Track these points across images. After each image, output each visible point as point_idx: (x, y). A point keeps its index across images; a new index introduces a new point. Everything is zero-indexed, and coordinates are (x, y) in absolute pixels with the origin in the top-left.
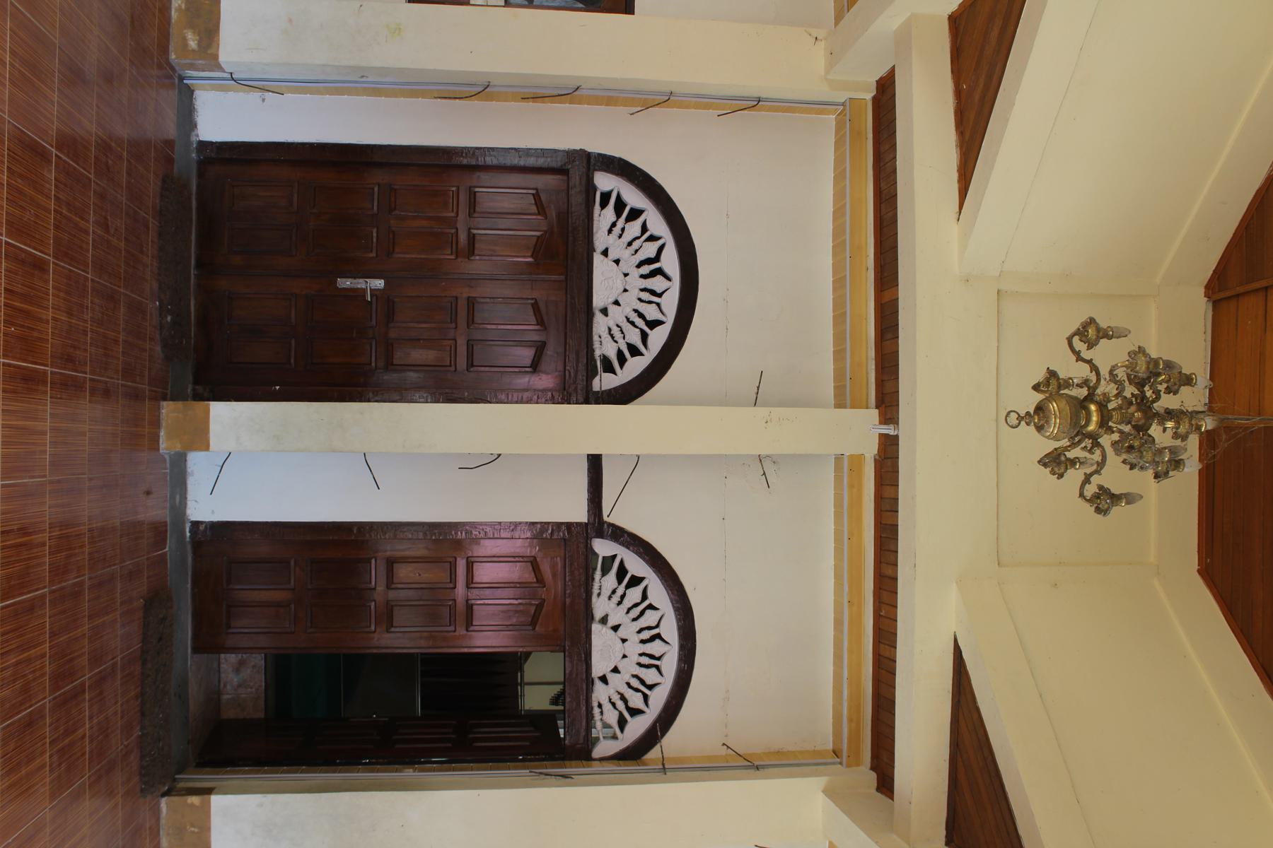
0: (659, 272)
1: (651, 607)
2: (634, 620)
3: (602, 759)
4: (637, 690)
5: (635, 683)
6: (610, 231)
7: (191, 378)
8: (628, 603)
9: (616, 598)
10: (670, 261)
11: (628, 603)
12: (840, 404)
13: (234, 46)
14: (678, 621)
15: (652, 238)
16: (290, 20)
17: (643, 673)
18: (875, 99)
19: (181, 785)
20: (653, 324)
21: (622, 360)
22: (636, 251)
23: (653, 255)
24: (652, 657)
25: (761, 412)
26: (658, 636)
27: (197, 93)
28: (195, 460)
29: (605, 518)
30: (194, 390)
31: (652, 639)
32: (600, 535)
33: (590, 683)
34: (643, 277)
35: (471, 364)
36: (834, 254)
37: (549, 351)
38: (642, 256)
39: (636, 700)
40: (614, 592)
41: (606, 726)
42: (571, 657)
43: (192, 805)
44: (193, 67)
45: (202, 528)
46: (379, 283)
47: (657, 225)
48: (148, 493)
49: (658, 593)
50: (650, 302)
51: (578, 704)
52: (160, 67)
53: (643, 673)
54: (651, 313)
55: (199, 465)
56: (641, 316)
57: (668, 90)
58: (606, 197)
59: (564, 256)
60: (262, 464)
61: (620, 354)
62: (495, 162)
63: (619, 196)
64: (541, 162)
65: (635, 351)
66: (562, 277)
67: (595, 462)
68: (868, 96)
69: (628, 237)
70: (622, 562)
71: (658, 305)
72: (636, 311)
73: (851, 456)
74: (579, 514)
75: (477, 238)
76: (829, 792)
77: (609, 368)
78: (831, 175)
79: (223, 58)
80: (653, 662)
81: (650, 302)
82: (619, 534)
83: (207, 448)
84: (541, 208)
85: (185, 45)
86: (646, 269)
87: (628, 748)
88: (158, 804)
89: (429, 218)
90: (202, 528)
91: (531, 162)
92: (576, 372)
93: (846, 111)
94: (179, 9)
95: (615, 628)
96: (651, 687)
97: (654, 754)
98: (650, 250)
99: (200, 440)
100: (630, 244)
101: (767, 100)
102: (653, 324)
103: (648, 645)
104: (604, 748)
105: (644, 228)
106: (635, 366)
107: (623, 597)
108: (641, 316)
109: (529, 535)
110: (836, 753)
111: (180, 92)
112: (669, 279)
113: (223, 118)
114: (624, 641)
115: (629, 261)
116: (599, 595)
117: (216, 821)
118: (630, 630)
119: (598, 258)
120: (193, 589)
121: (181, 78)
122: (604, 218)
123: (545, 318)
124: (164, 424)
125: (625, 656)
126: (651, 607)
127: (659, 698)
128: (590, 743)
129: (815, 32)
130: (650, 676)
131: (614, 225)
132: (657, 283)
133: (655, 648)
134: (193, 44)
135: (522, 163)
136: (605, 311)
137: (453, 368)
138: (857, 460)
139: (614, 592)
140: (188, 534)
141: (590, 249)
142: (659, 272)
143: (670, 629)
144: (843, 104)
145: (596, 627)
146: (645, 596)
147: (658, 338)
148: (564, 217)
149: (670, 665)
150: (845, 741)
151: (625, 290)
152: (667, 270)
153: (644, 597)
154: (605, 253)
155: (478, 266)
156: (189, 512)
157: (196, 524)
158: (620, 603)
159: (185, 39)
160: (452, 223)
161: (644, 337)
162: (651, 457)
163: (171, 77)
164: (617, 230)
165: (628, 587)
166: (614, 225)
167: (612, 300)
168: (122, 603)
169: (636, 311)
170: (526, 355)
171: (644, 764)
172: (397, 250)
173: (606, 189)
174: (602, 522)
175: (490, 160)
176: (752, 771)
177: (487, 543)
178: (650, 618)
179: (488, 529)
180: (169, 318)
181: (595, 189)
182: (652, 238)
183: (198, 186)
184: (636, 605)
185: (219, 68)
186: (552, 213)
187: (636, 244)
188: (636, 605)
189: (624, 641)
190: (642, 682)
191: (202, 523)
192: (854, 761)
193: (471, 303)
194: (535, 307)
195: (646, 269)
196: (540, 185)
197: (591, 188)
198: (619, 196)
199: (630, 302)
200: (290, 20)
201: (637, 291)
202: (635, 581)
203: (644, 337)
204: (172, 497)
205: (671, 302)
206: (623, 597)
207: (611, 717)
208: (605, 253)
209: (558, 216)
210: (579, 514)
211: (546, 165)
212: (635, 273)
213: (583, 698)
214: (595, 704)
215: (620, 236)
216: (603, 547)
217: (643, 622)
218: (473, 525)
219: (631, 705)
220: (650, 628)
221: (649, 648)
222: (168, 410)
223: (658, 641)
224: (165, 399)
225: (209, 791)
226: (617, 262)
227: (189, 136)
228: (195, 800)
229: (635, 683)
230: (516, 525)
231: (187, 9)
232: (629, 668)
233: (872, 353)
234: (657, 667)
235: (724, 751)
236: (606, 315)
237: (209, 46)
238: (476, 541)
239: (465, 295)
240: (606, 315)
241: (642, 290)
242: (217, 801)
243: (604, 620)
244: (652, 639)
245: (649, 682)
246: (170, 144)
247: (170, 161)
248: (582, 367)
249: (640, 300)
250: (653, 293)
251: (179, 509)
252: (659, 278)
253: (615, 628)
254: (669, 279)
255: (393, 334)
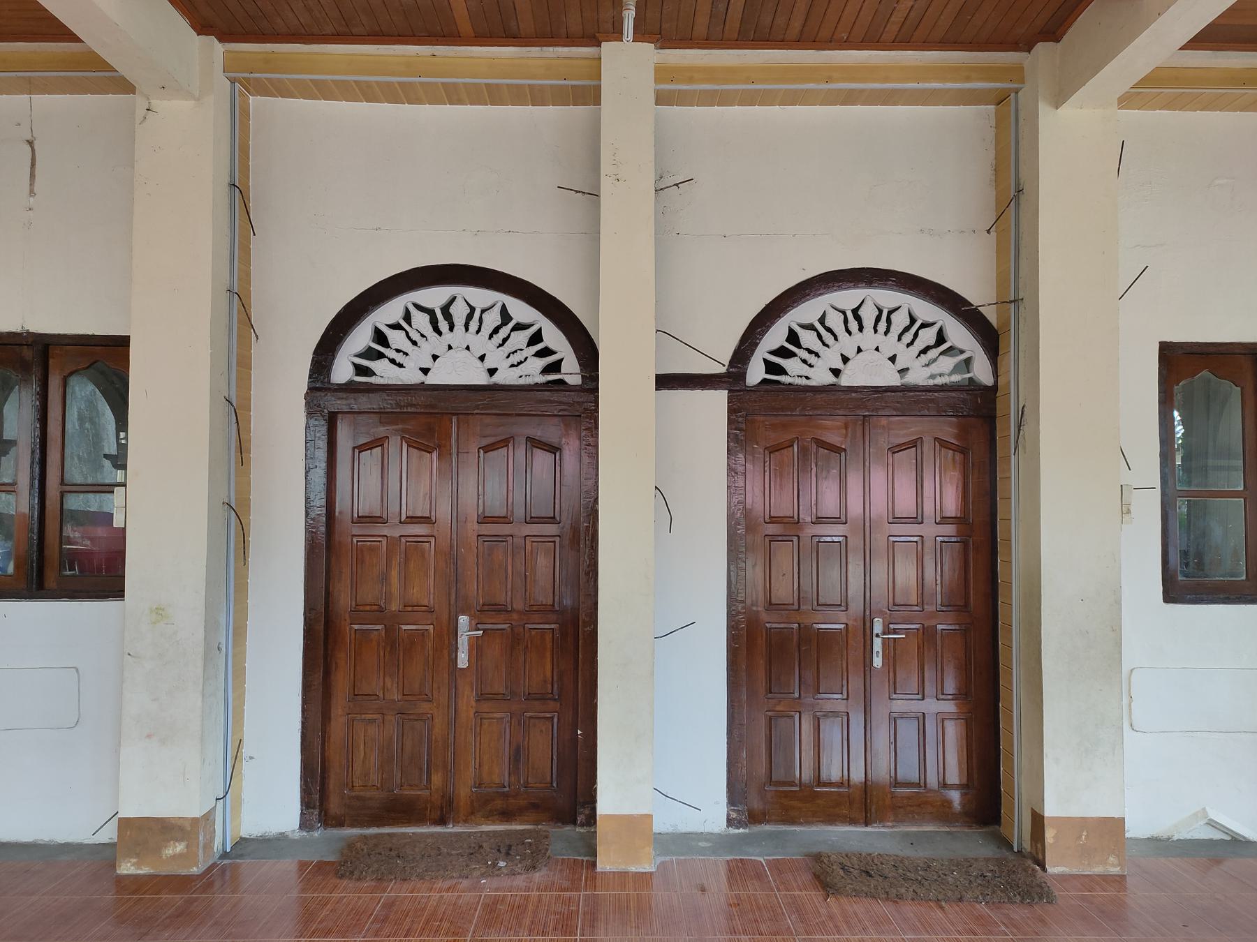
0: (446, 310)
1: (822, 320)
2: (836, 338)
3: (996, 373)
4: (916, 335)
5: (908, 337)
6: (400, 366)
7: (568, 828)
8: (816, 345)
9: (812, 359)
10: (434, 296)
11: (816, 345)
12: (597, 100)
13: (181, 802)
14: (840, 288)
15: (407, 317)
16: (149, 736)
17: (896, 329)
18: (222, 39)
19: (1027, 845)
20: (505, 316)
21: (546, 352)
22: (423, 336)
23: (427, 317)
24: (878, 319)
25: (606, 186)
26: (855, 312)
27: (244, 833)
28: (659, 826)
29: (723, 370)
30: (582, 825)
31: (858, 318)
32: (742, 376)
33: (905, 389)
34: (451, 329)
35: (552, 520)
36: (418, 101)
37: (537, 433)
38: (428, 329)
39: (928, 336)
40: (804, 361)
41: (956, 370)
42: (877, 410)
43: (1055, 837)
44: (208, 845)
45: (734, 815)
46: (463, 620)
47: (390, 311)
48: (703, 890)
49: (807, 312)
50: (481, 320)
51: (932, 401)
52: (210, 885)
53: (896, 329)
54: (493, 319)
55: (668, 820)
56: (496, 331)
57: (225, 296)
58: (361, 370)
59: (432, 417)
60: (663, 755)
61: (539, 354)
62: (323, 495)
63: (359, 356)
64: (322, 443)
65: (536, 338)
66: (454, 419)
67: (665, 382)
68: (218, 48)
69: (406, 346)
70: (772, 353)
71: (483, 311)
72: (491, 337)
73: (657, 80)
74: (718, 399)
75: (410, 514)
76: (1059, 100)
77: (555, 367)
78: (322, 104)
79: (197, 814)
80: (884, 317)
81: (481, 320)
82: (742, 355)
83: (650, 816)
84: (378, 443)
85: (181, 855)
86: (443, 325)
87: (983, 345)
88: (1052, 876)
89: (389, 565)
90: (734, 815)
91: (322, 455)
92: (561, 403)
93: (246, 83)
94: (138, 865)
95: (845, 360)
96: (913, 320)
97: (991, 315)
98: (421, 320)
99: (637, 825)
100: (415, 343)
101: (232, 176)
102: (505, 316)
103: (865, 323)
104: (982, 371)
105: (396, 327)
106: (554, 337)
107: (810, 352)
108: (496, 331)
109: (741, 455)
110: (1001, 99)
111: (241, 856)
112: (453, 299)
113: (272, 801)
114: (859, 350)
115: (434, 343)
116: (807, 378)
117: (1075, 811)
118: (847, 344)
119: (431, 379)
120: (801, 824)
121: (225, 855)
122: (384, 372)
123: (499, 438)
124: (622, 868)
125: (877, 349)
126: (822, 320)
127: (926, 310)
128: (972, 386)
129: (141, 112)
130: (900, 320)
131: (393, 361)
132: (459, 312)
133: (868, 315)
134: (180, 848)
135: (324, 465)
136: (492, 372)
137: (557, 539)
138: (662, 73)
139: (804, 361)
140: (741, 830)
141: (422, 387)
142: (446, 310)
143: (847, 298)
144: (232, 83)
145: (845, 381)
146: (810, 327)
147: (521, 311)
148: (384, 416)
149: (888, 297)
150: (992, 85)
151: (468, 348)
152: (443, 300)
153: (810, 327)
154: (425, 371)
155: (444, 511)
156: (716, 830)
157: (730, 822)
158: (817, 355)
159: (174, 857)
160: (393, 542)
161: (519, 327)
162: (658, 316)
163: (223, 870)
164: (399, 358)
165: (799, 346)
166: (393, 361)
167: (479, 362)
168: (839, 933)
169: (491, 337)
170: (542, 460)
171: (1007, 323)
172: (425, 603)
173: (351, 369)
174: (728, 375)
175: (320, 501)
176: (1023, 198)
177: (749, 501)
178: (835, 321)
179: (735, 500)
180: (502, 864)
181: (351, 382)
182: (407, 317)
183: (352, 826)
184: (820, 337)
185: (208, 817)
186: (382, 431)
187: (415, 336)
188: (820, 337)
189: (859, 350)
190: (907, 329)
191: (728, 815)
192: (1017, 74)
193: (484, 520)
194: (488, 449)
195: (443, 325)
196: (350, 445)
197: (349, 388)
198: (359, 356)
199: (481, 343)
200: (149, 736)
201: (468, 334)
202: (793, 337)
203: (519, 327)
204: (702, 851)
205: (481, 297)
206: (810, 352)
207: (947, 363)
208: (425, 371)
209: (382, 423)
210: (718, 399)
211: (325, 438)
212: (448, 337)
213: (923, 396)
214: (931, 382)
215: (406, 354)
216: (756, 373)
217: (839, 329)
218: (731, 516)
219: (932, 342)
220: (846, 321)
221: (868, 322)
222: (606, 862)
223: (861, 312)
224: (594, 865)
225: (1038, 820)
226: (435, 357)
227: (294, 841)
228: (1049, 835)
229: (908, 337)
230: (731, 471)
231: (137, 855)
232: (890, 344)
233: (534, 51)
234: (890, 313)
235: (993, 233)
236: (496, 370)
237: (181, 829)
238: (747, 513)
239: (476, 526)
240: (496, 370)
241: (467, 329)
242: (1051, 810)
243: (836, 372)
244: (858, 318)
245: (907, 322)
246: (303, 866)
247: (321, 867)
248: (556, 397)
249: (478, 332)
250: (470, 317)
251: (719, 843)
252: (452, 310)
253: (845, 360)
254: (453, 299)
255: (519, 605)
